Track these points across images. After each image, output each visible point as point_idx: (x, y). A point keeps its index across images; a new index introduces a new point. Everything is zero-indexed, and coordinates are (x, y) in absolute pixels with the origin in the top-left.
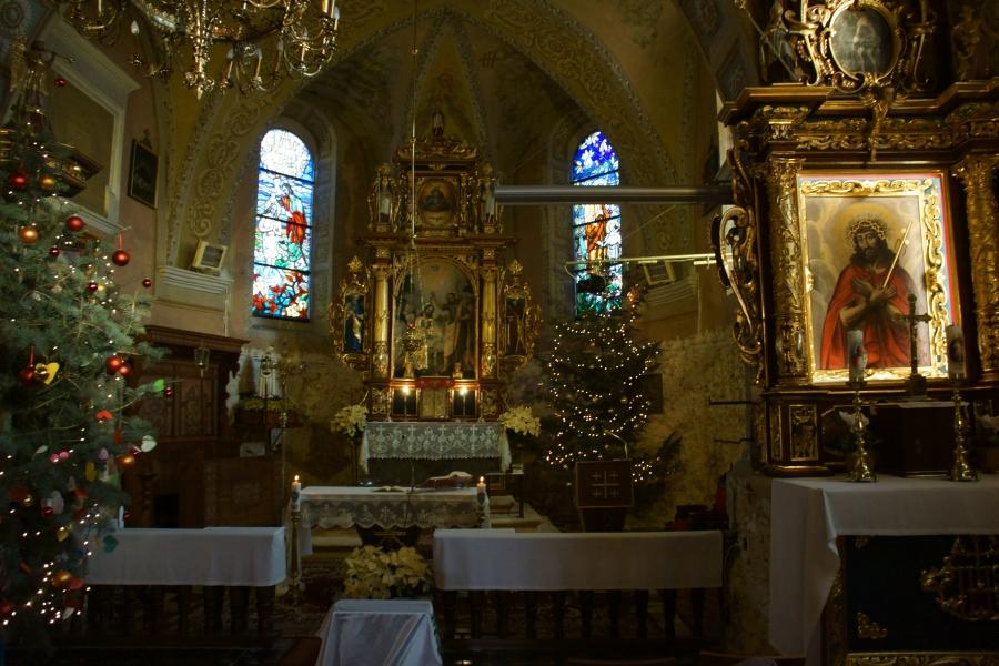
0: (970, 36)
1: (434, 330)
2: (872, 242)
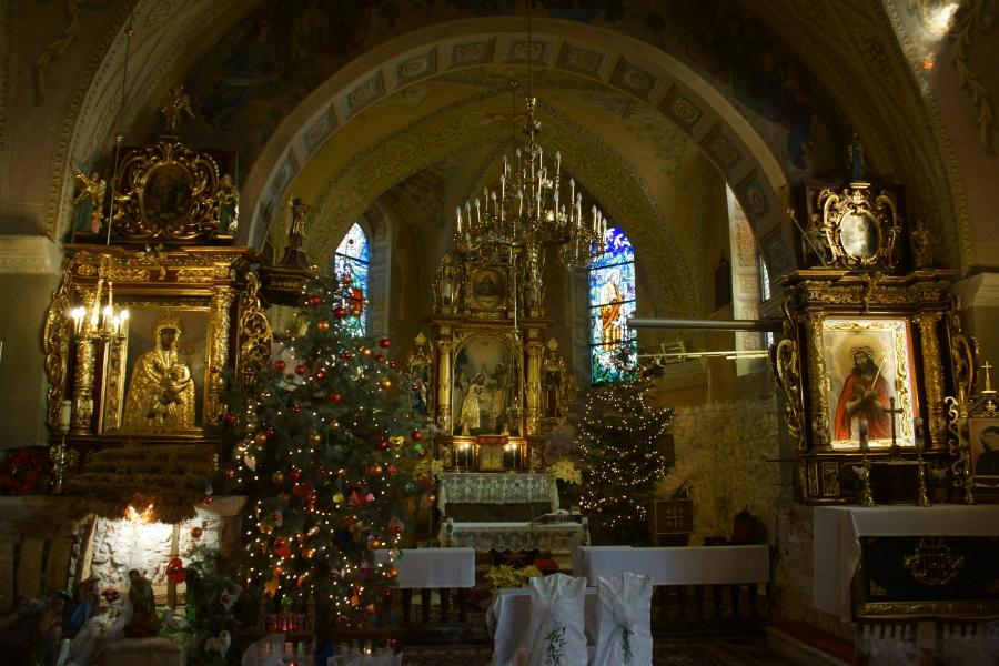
0: (922, 240)
1: (485, 396)
2: (865, 360)
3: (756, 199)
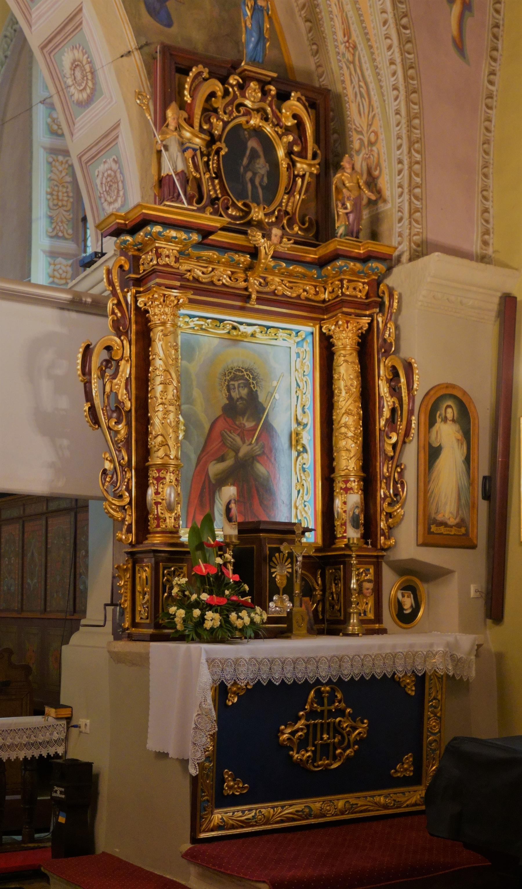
2: (244, 392)
3: (78, 74)
